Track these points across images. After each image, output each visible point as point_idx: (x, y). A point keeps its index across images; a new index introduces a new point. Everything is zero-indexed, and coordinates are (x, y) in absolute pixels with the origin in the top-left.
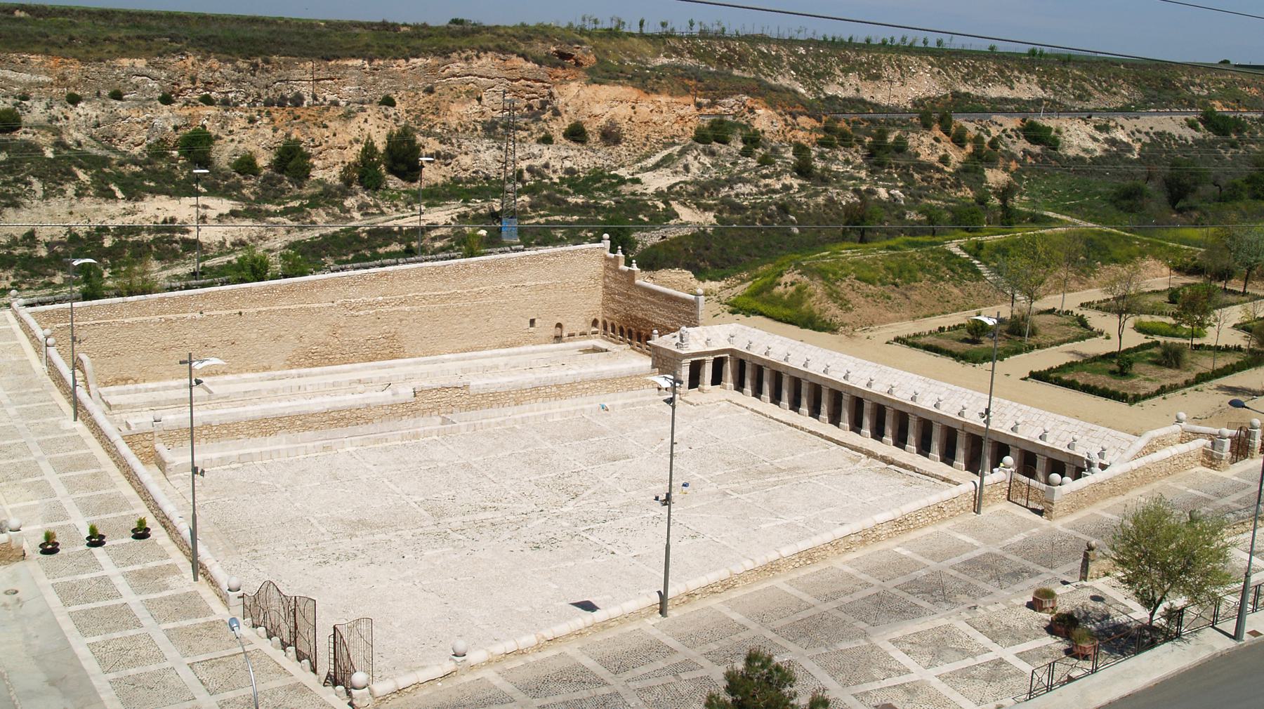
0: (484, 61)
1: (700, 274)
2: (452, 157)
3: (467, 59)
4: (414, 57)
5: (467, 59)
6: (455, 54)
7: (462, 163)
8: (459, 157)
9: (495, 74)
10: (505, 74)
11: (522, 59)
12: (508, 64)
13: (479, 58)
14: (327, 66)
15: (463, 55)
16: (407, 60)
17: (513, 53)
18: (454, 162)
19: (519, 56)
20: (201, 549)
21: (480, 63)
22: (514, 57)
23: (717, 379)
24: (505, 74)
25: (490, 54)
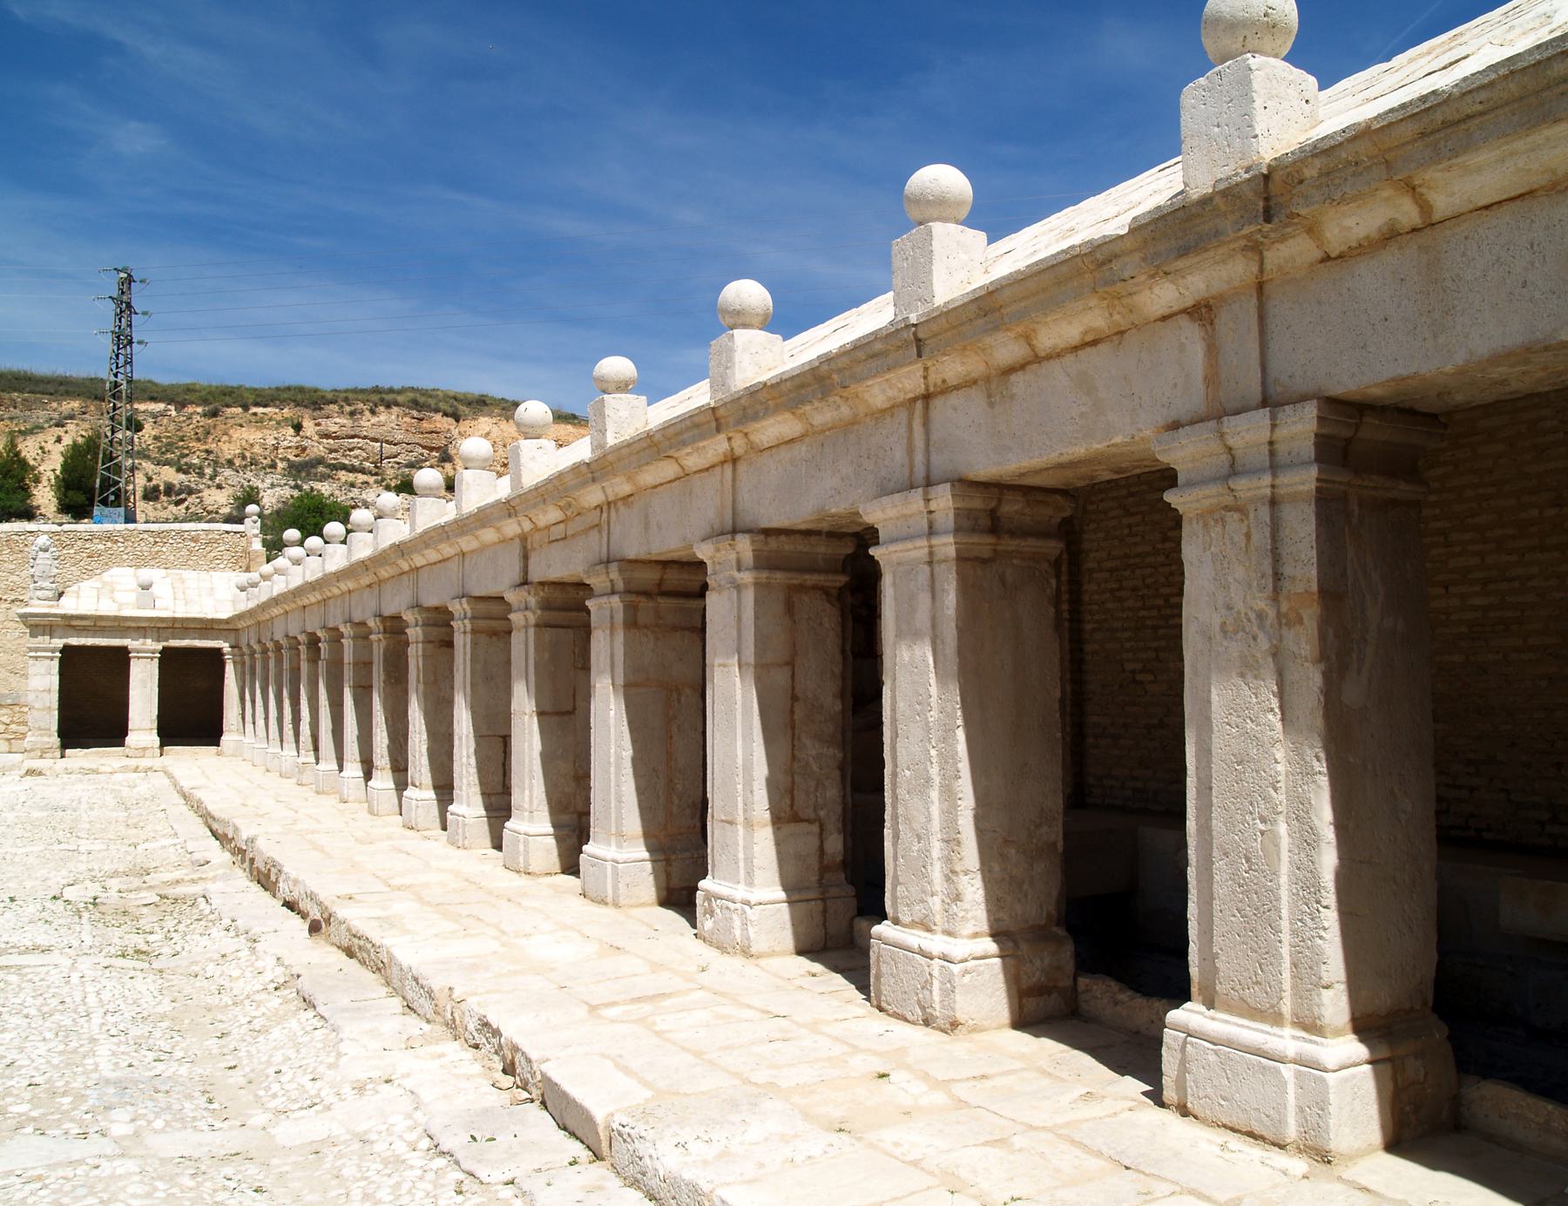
0: (383, 418)
1: (1064, 519)
2: (191, 492)
3: (352, 414)
4: (257, 404)
5: (352, 414)
6: (334, 407)
7: (208, 501)
8: (205, 493)
9: (399, 437)
10: (417, 438)
11: (450, 420)
12: (426, 425)
13: (373, 412)
14: (99, 408)
15: (348, 409)
16: (246, 408)
17: (437, 411)
18: (192, 499)
19: (446, 414)
20: (1050, 1135)
21: (374, 420)
22: (438, 417)
23: (439, 619)
24: (417, 438)
25: (395, 409)
